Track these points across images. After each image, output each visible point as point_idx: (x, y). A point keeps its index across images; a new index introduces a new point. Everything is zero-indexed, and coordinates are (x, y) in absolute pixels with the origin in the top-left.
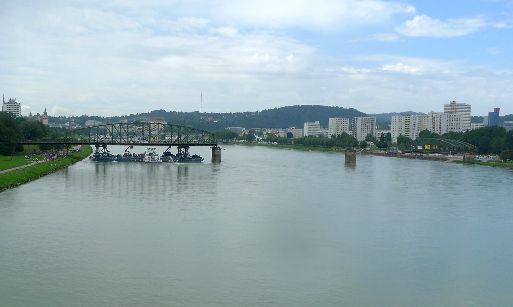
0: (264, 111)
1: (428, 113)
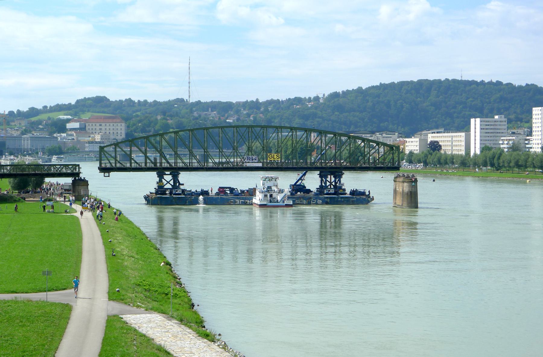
0: (335, 95)
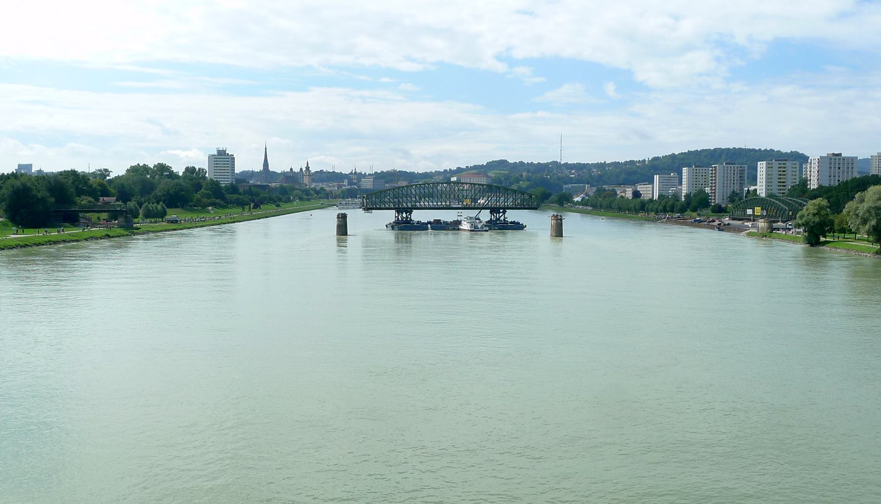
0: (656, 159)
1: (871, 156)
